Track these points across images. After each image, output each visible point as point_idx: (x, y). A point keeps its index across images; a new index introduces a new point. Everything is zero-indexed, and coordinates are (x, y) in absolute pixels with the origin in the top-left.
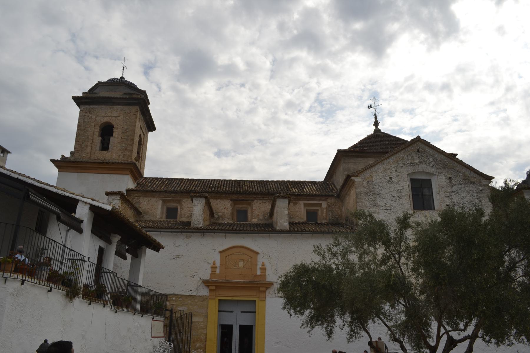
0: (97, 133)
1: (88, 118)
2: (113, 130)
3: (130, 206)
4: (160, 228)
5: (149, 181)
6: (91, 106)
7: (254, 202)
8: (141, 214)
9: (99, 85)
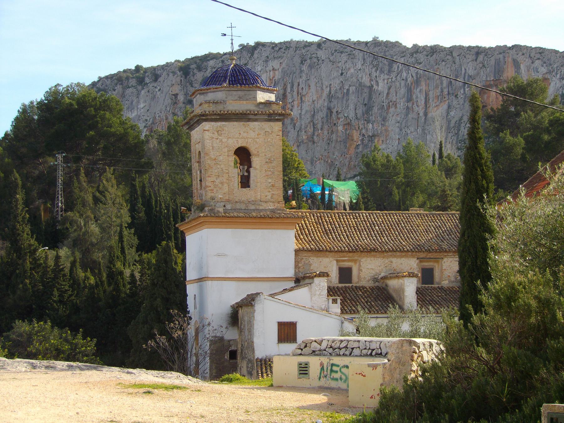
1: (218, 141)
7: (444, 260)
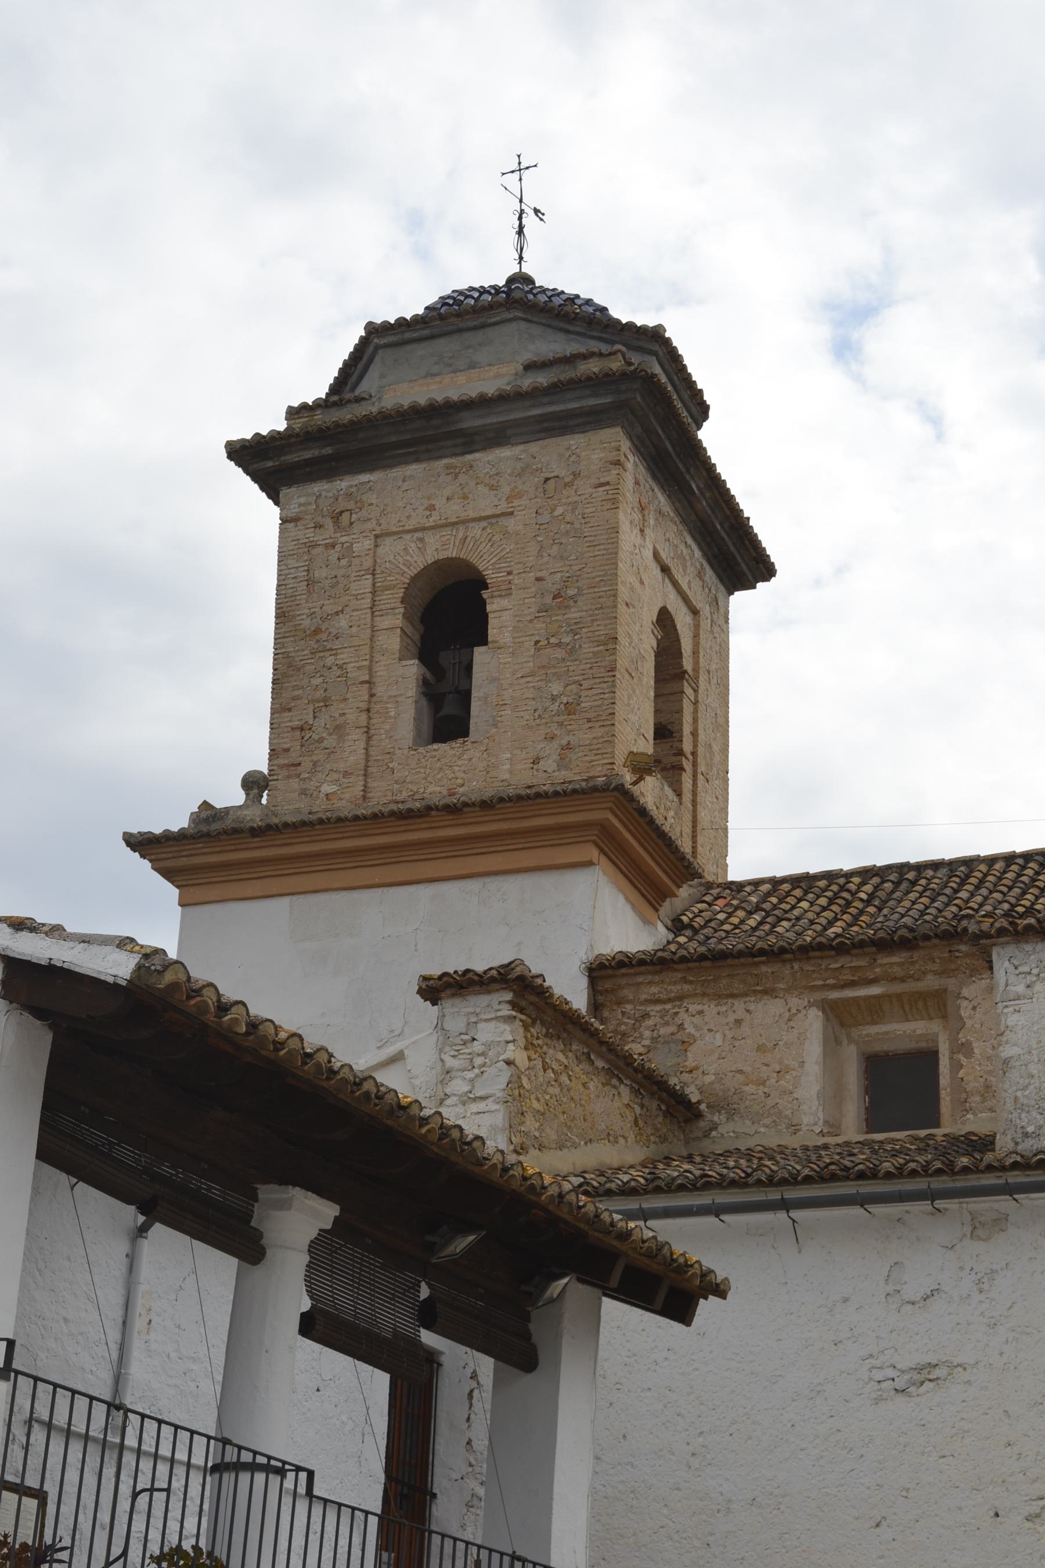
0: (392, 642)
1: (333, 555)
2: (483, 603)
3: (600, 1064)
4: (784, 1182)
5: (754, 899)
6: (344, 484)
8: (699, 1115)
9: (377, 348)
